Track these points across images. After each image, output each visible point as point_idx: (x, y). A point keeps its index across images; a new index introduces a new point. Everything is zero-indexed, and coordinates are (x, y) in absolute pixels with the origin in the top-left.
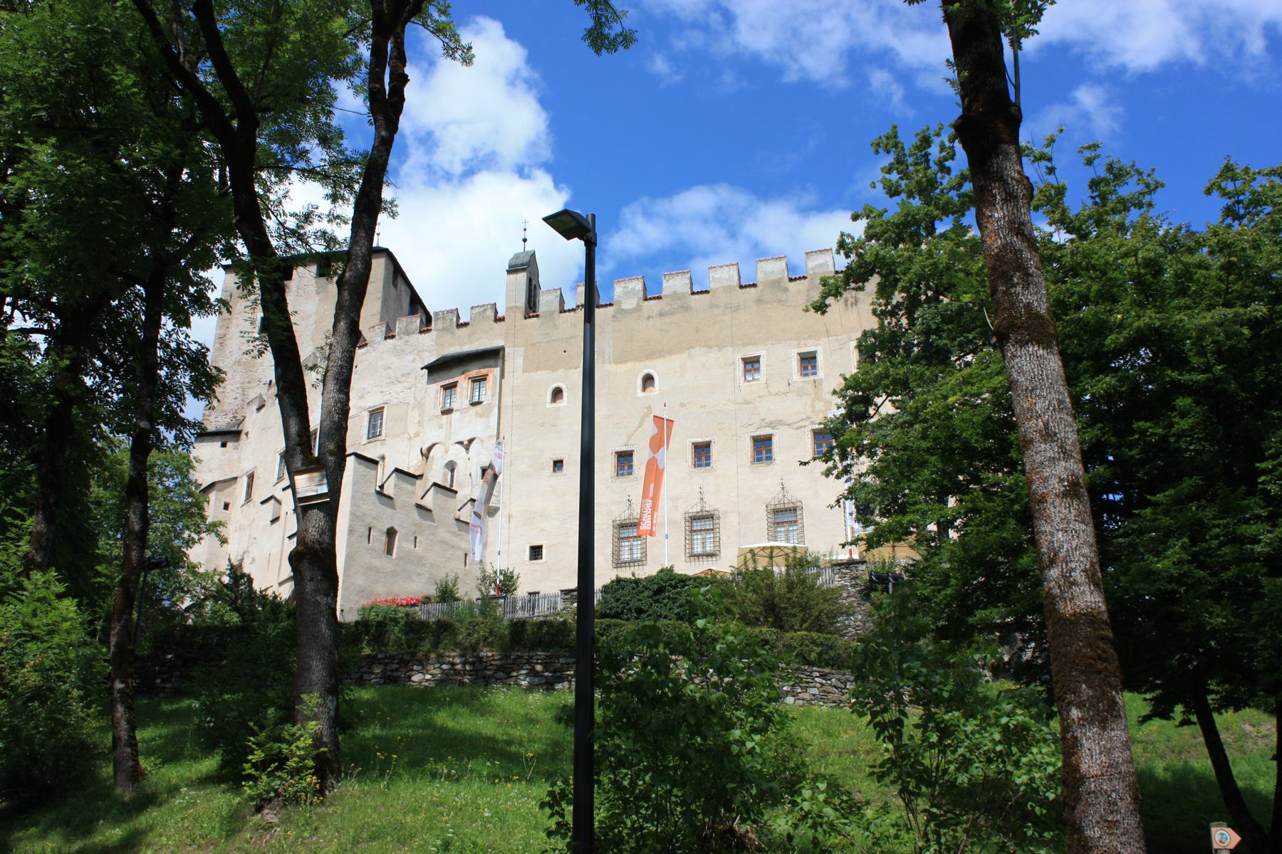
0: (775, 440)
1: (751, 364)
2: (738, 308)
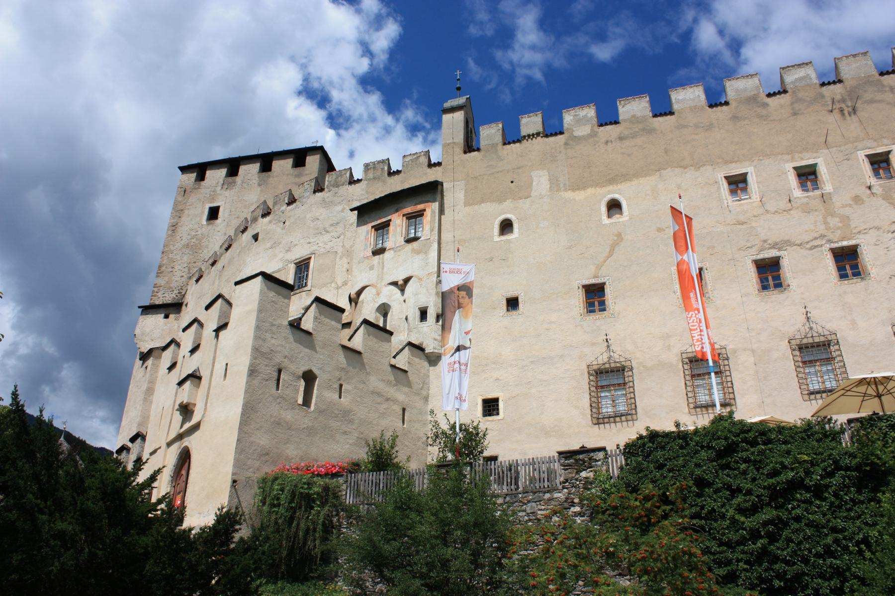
0: (785, 263)
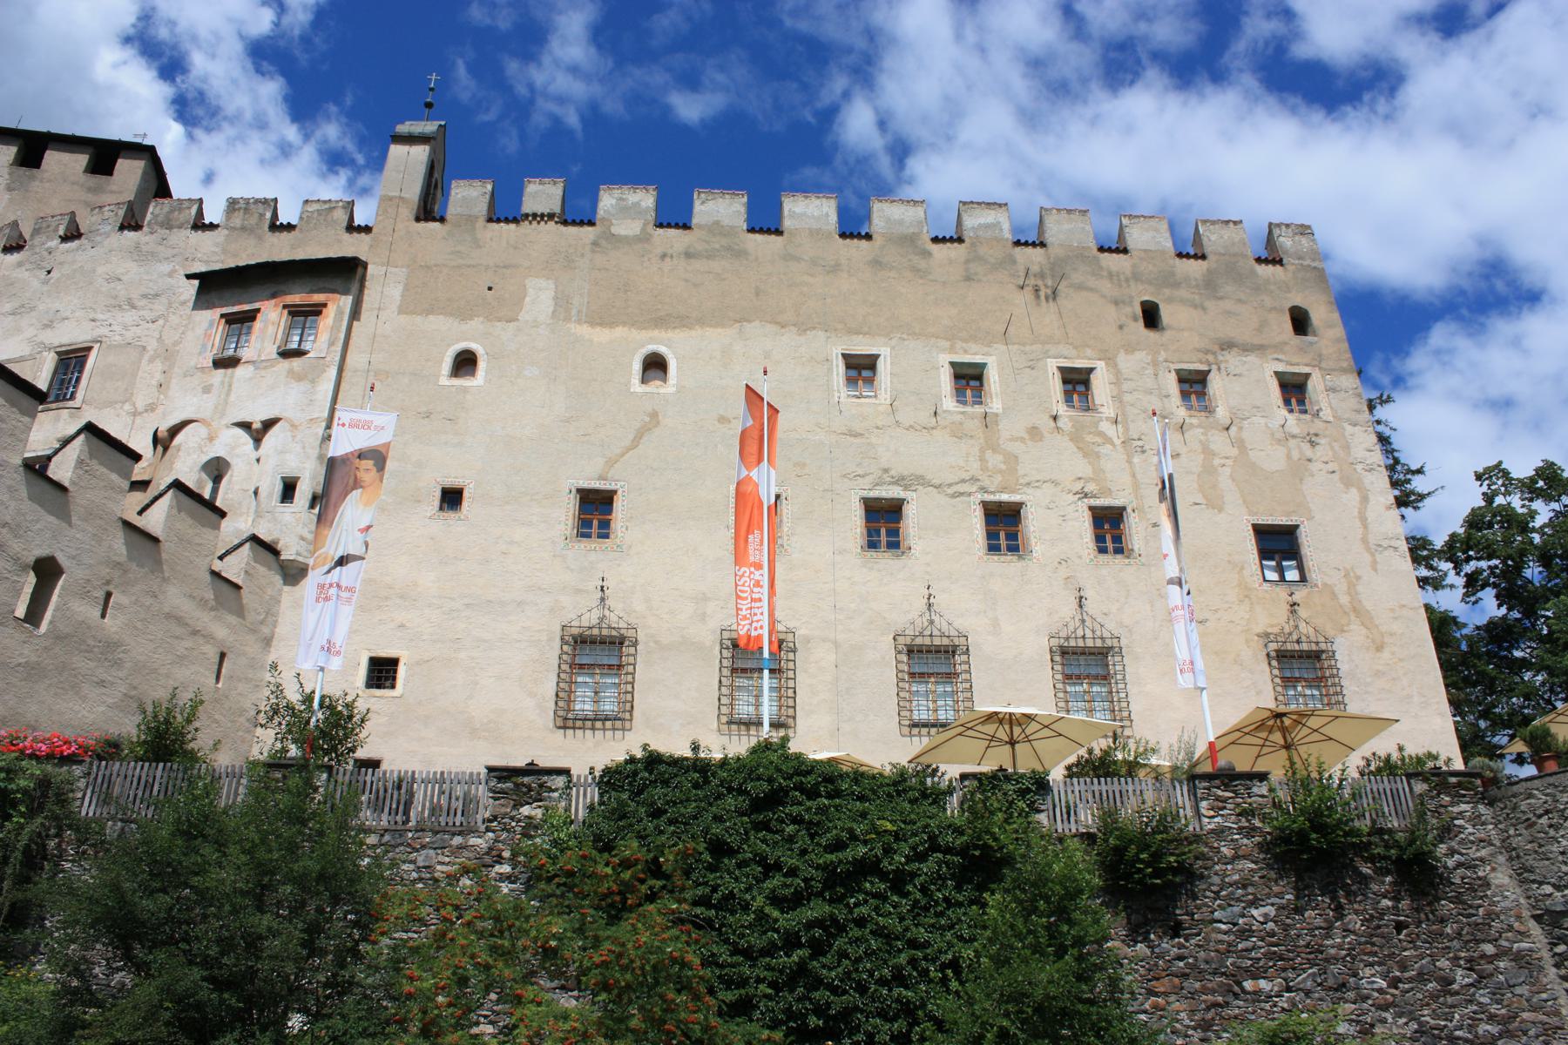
0: (910, 511)
1: (861, 368)
2: (835, 269)
